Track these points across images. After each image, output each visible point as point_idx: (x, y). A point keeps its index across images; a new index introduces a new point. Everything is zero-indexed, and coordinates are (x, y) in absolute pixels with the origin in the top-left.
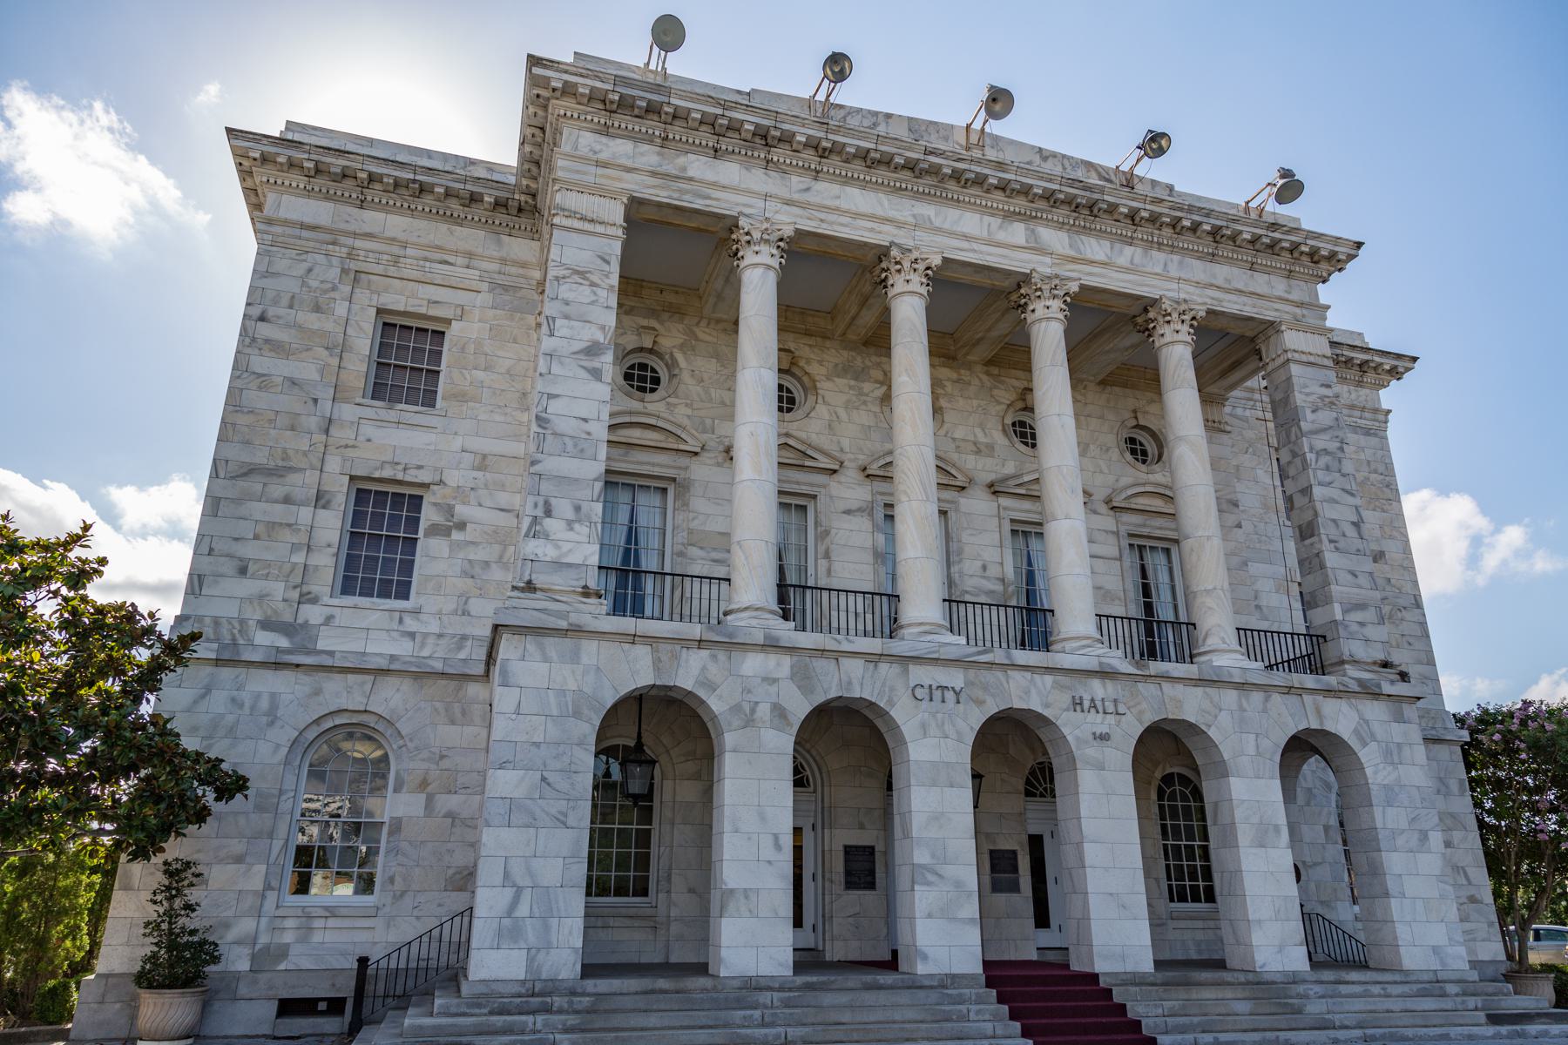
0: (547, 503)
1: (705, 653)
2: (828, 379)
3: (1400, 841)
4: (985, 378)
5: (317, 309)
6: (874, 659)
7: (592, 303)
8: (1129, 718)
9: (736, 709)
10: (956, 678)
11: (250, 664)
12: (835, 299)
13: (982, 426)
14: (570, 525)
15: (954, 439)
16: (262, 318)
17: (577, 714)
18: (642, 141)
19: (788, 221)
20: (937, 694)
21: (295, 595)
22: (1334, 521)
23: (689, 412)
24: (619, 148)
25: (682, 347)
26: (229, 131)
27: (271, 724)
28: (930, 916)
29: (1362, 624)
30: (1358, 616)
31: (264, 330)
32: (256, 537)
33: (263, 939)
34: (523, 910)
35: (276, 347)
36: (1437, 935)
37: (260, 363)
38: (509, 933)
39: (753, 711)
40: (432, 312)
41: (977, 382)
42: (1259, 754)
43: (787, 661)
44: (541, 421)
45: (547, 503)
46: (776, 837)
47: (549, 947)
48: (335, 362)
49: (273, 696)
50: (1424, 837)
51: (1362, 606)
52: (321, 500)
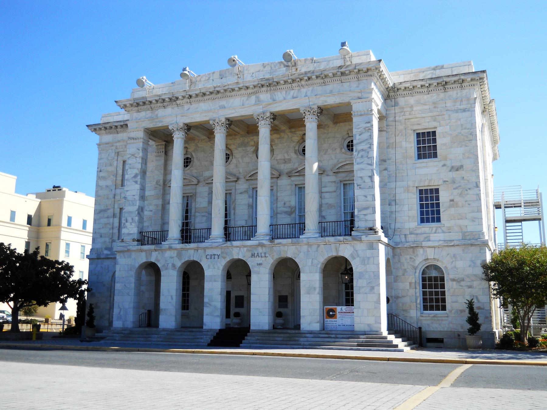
1: (157, 253)
2: (236, 149)
3: (362, 290)
4: (289, 134)
5: (111, 165)
7: (136, 163)
8: (269, 257)
9: (164, 266)
11: (103, 258)
13: (287, 152)
15: (277, 160)
16: (100, 171)
17: (131, 270)
18: (147, 110)
20: (213, 257)
21: (111, 241)
22: (361, 177)
23: (196, 171)
24: (143, 114)
25: (194, 151)
26: (87, 126)
28: (207, 315)
29: (365, 215)
31: (102, 174)
34: (122, 313)
41: (286, 136)
42: (312, 265)
43: (176, 252)
48: (115, 179)
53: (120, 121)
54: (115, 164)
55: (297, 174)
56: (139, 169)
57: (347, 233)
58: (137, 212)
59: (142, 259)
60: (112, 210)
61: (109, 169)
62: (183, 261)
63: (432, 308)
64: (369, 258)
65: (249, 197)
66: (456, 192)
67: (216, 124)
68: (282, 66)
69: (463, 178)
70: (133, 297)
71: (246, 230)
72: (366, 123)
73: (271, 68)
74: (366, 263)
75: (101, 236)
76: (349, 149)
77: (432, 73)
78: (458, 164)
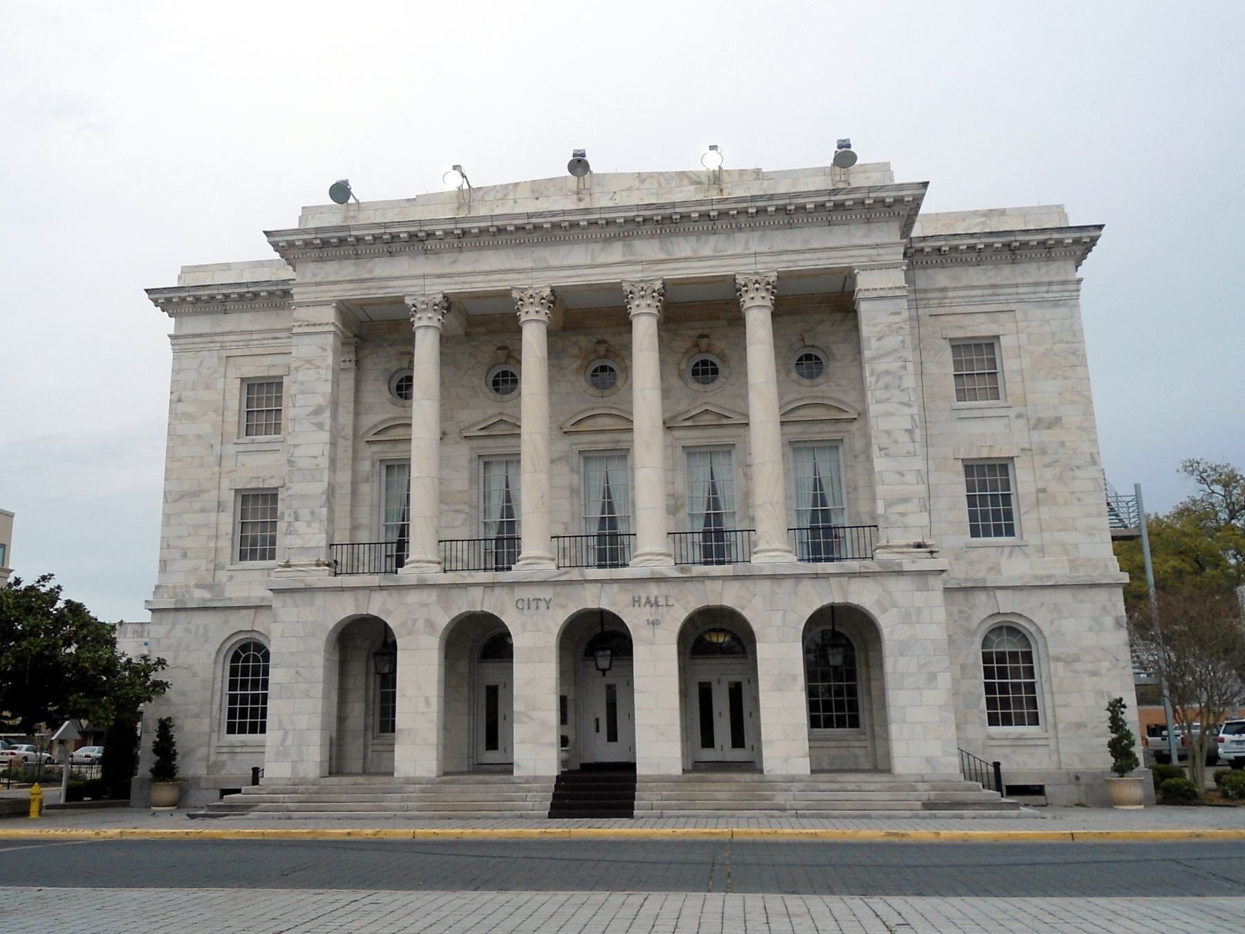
0: (296, 513)
5: (208, 387)
6: (491, 586)
10: (546, 593)
12: (482, 332)
14: (309, 524)
16: (179, 401)
17: (314, 635)
19: (437, 289)
20: (533, 605)
22: (888, 432)
27: (206, 641)
28: (522, 742)
29: (903, 515)
30: (901, 508)
31: (182, 407)
32: (189, 535)
33: (213, 758)
34: (289, 742)
35: (189, 417)
36: (933, 749)
37: (181, 429)
38: (282, 754)
39: (414, 625)
40: (272, 374)
44: (291, 462)
45: (296, 513)
46: (427, 699)
47: (302, 761)
48: (220, 419)
49: (205, 626)
50: (932, 677)
51: (905, 500)
52: (220, 507)
53: (240, 285)
54: (220, 384)
55: (690, 423)
56: (328, 397)
57: (488, 566)
58: (324, 497)
59: (346, 608)
60: (214, 494)
61: (204, 395)
62: (455, 613)
63: (1007, 721)
64: (919, 610)
65: (572, 470)
66: (1049, 473)
67: (527, 301)
68: (686, 182)
69: (1064, 443)
70: (321, 701)
71: (567, 545)
72: (892, 314)
73: (660, 184)
74: (914, 619)
75: (185, 555)
76: (401, 395)
77: (983, 223)
78: (1049, 414)
